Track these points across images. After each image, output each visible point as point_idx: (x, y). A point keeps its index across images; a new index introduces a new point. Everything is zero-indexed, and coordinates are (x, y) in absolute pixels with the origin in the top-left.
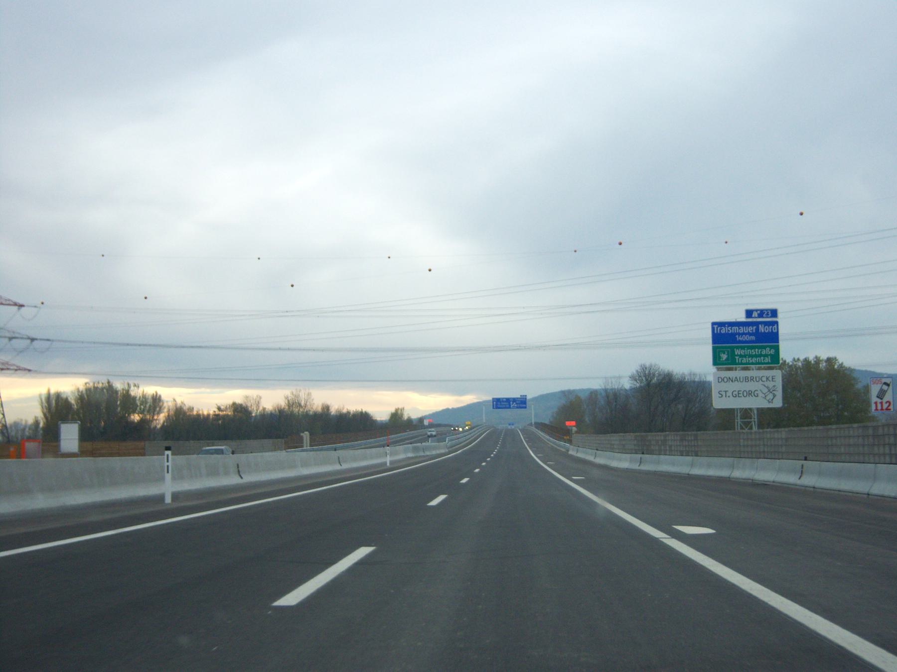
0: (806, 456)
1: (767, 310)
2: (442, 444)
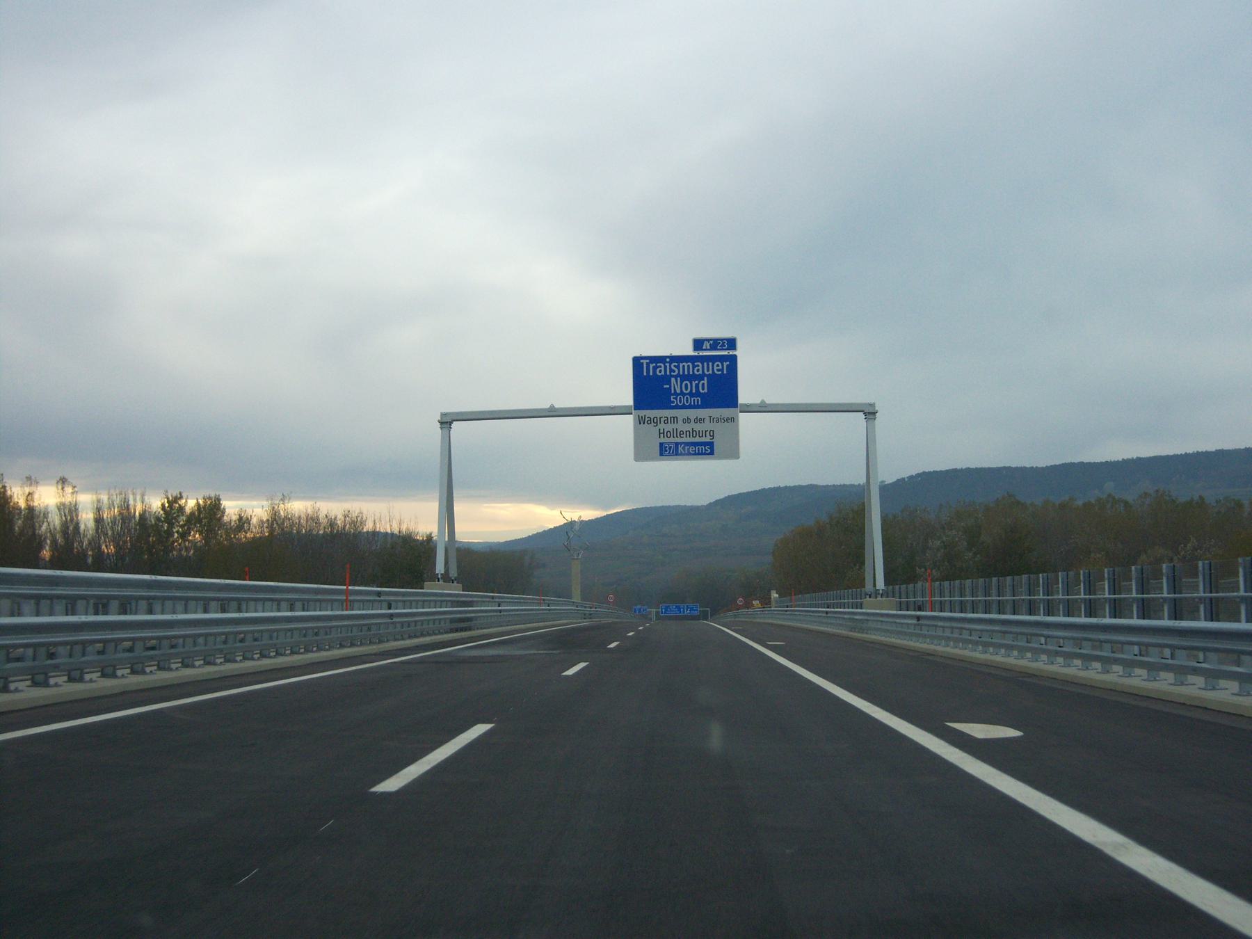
1: (722, 340)
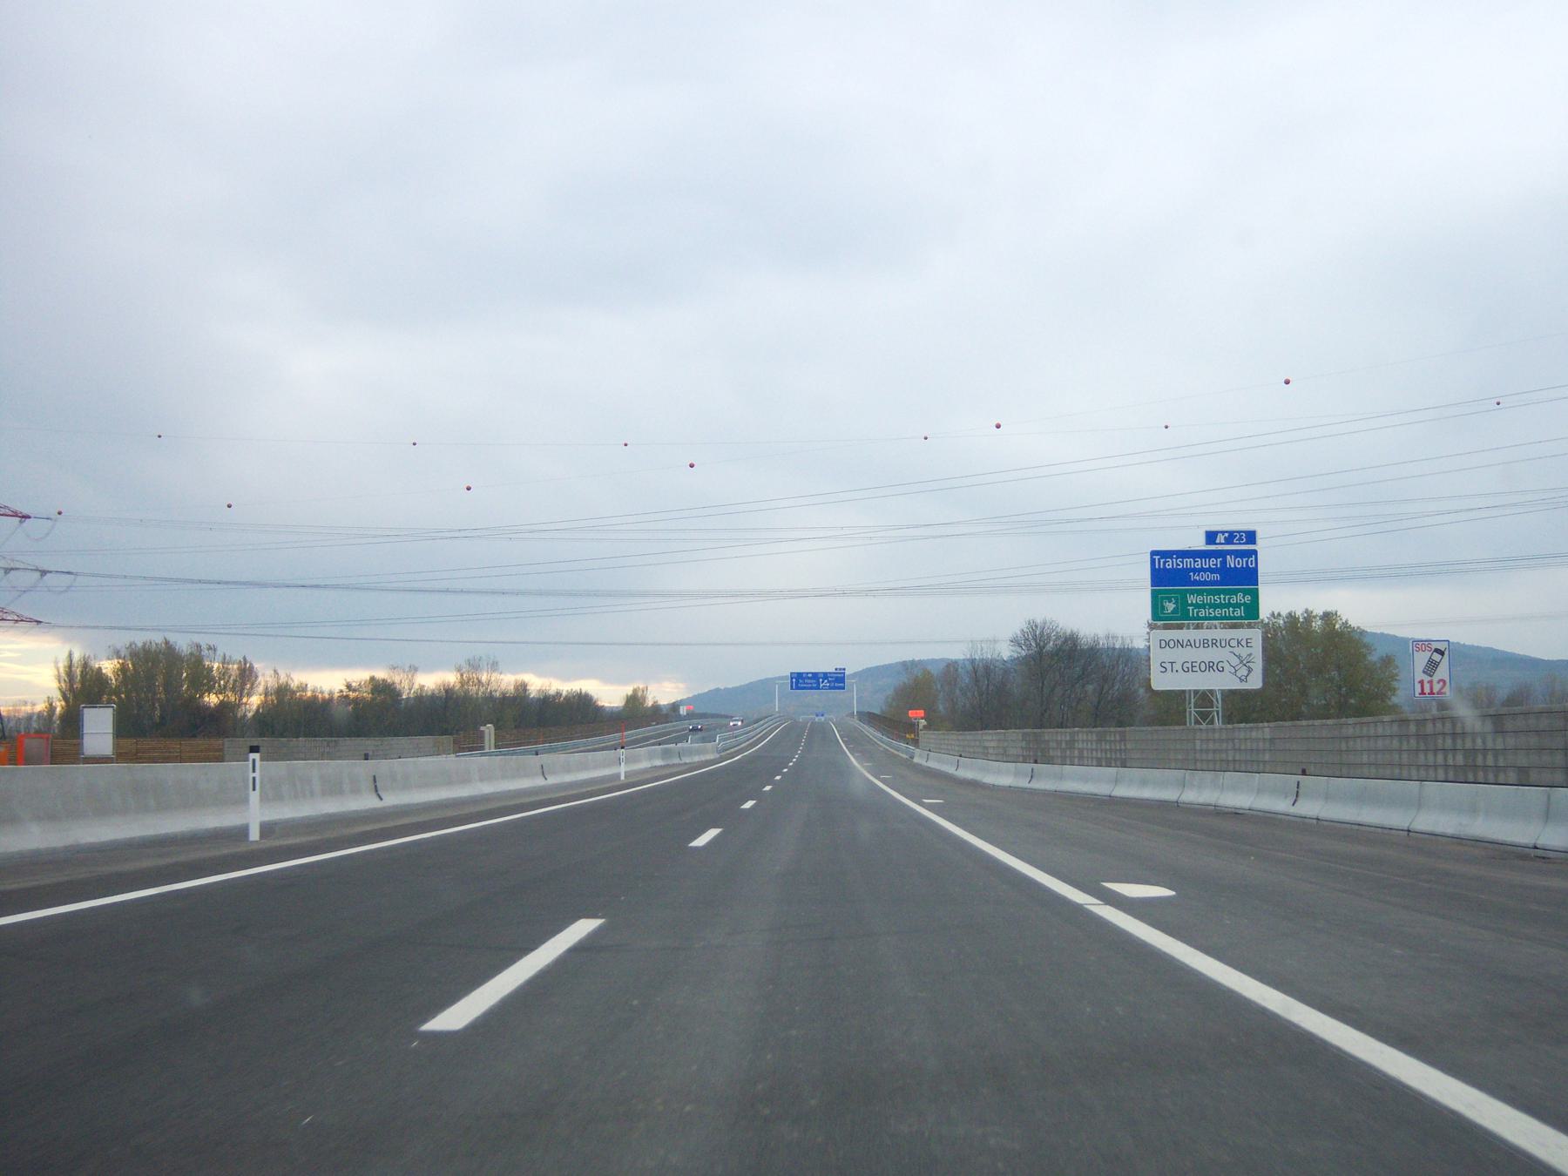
0: (1305, 767)
2: (709, 745)
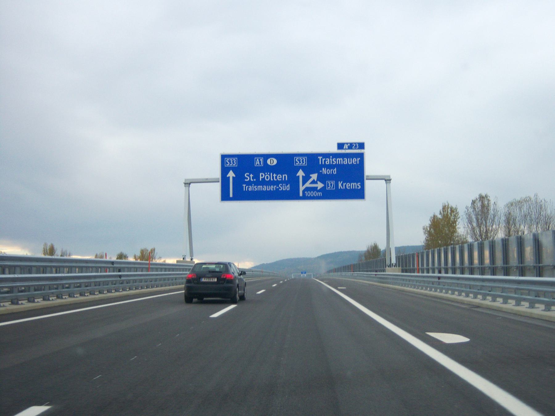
1: (355, 143)
